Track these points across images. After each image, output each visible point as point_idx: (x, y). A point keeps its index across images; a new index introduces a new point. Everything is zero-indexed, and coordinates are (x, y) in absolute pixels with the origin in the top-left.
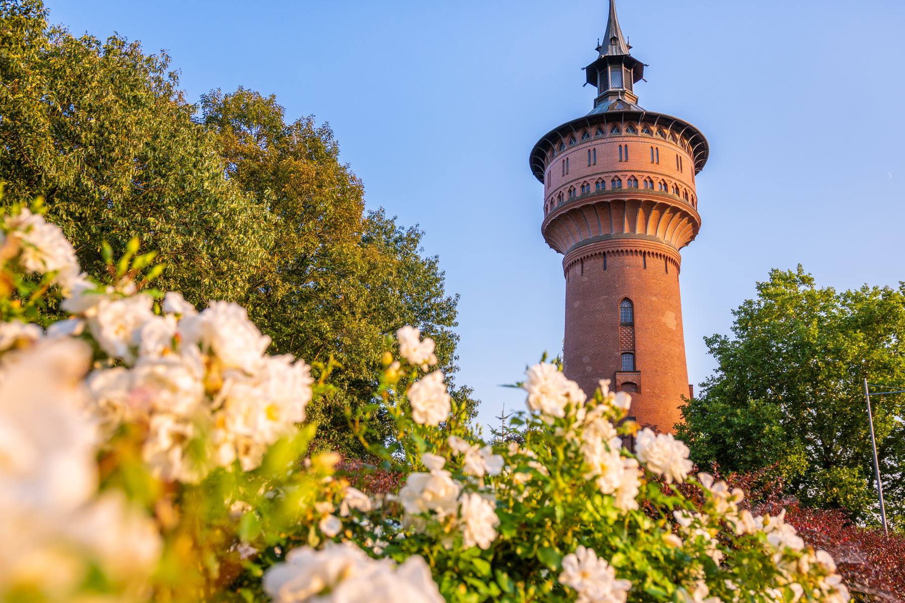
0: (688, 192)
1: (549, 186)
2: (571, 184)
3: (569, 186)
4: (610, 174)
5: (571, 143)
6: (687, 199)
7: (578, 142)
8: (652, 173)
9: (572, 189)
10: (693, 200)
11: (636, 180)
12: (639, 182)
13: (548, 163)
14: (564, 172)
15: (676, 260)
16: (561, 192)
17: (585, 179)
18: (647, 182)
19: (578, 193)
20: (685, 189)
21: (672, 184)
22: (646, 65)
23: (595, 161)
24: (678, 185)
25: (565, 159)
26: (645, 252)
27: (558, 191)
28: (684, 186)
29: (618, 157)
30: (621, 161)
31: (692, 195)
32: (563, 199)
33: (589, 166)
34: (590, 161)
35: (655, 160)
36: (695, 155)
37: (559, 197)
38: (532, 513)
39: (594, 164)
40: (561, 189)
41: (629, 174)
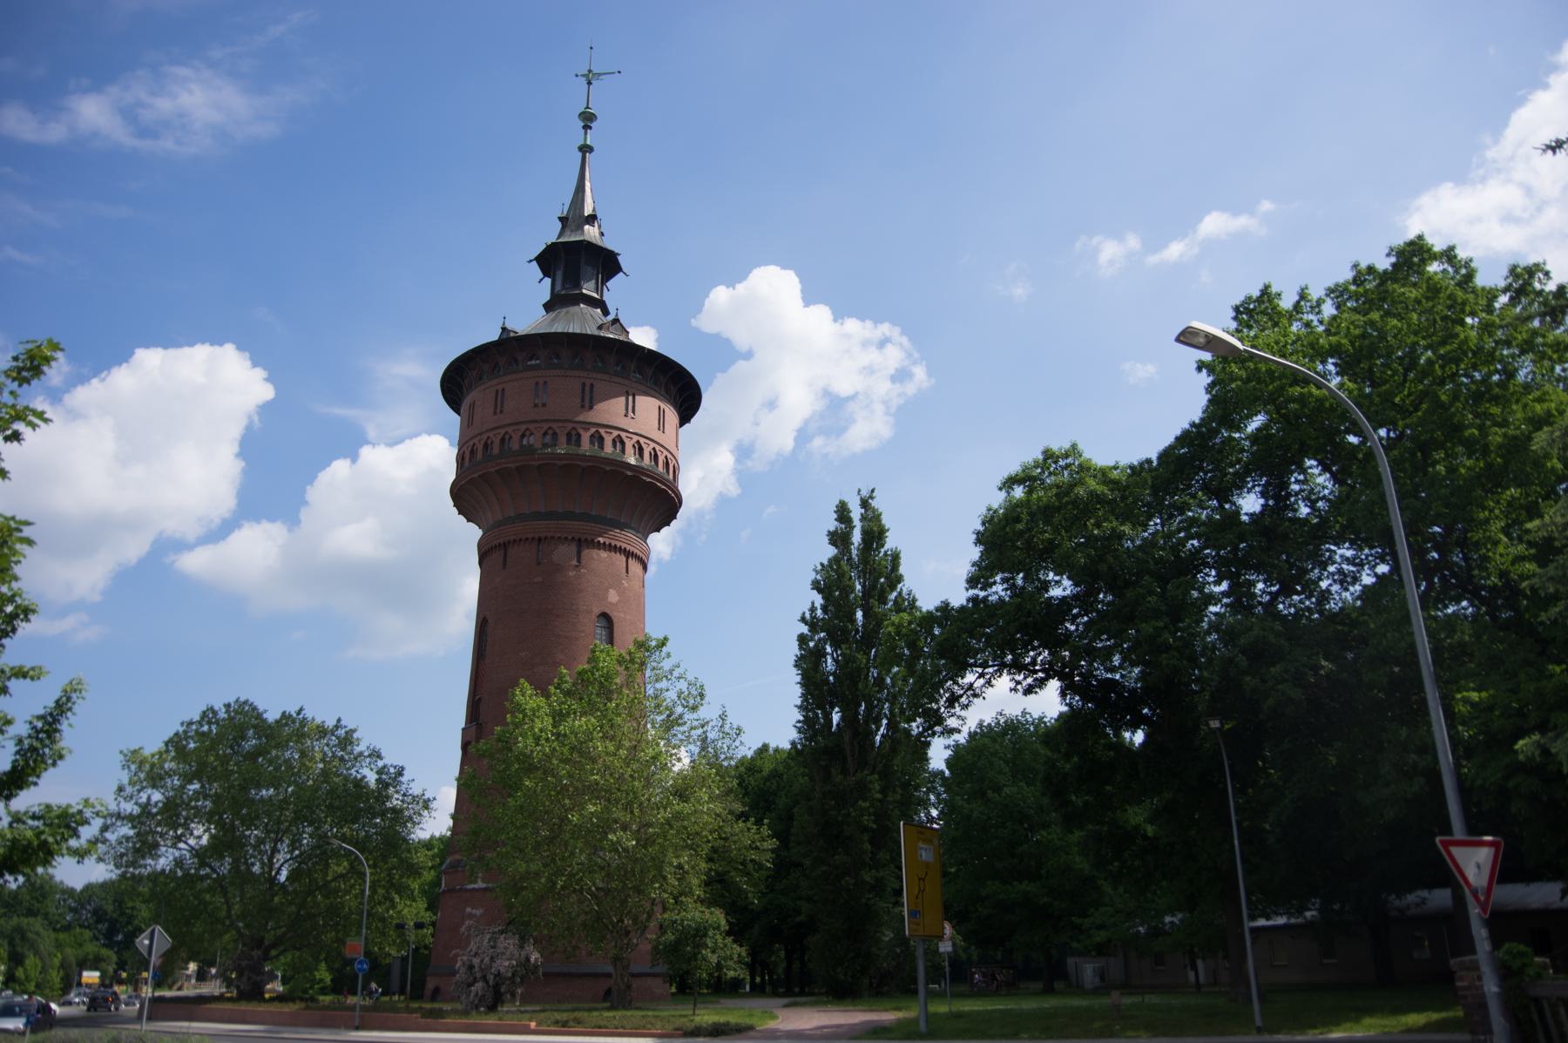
0: (659, 453)
2: (506, 429)
3: (502, 431)
6: (657, 463)
8: (662, 446)
9: (507, 437)
10: (667, 464)
11: (623, 443)
14: (496, 408)
15: (641, 555)
20: (654, 449)
21: (650, 449)
25: (500, 390)
26: (580, 539)
27: (471, 443)
28: (665, 453)
30: (583, 406)
31: (666, 457)
32: (492, 449)
36: (681, 406)
37: (486, 445)
38: (331, 980)
41: (616, 433)
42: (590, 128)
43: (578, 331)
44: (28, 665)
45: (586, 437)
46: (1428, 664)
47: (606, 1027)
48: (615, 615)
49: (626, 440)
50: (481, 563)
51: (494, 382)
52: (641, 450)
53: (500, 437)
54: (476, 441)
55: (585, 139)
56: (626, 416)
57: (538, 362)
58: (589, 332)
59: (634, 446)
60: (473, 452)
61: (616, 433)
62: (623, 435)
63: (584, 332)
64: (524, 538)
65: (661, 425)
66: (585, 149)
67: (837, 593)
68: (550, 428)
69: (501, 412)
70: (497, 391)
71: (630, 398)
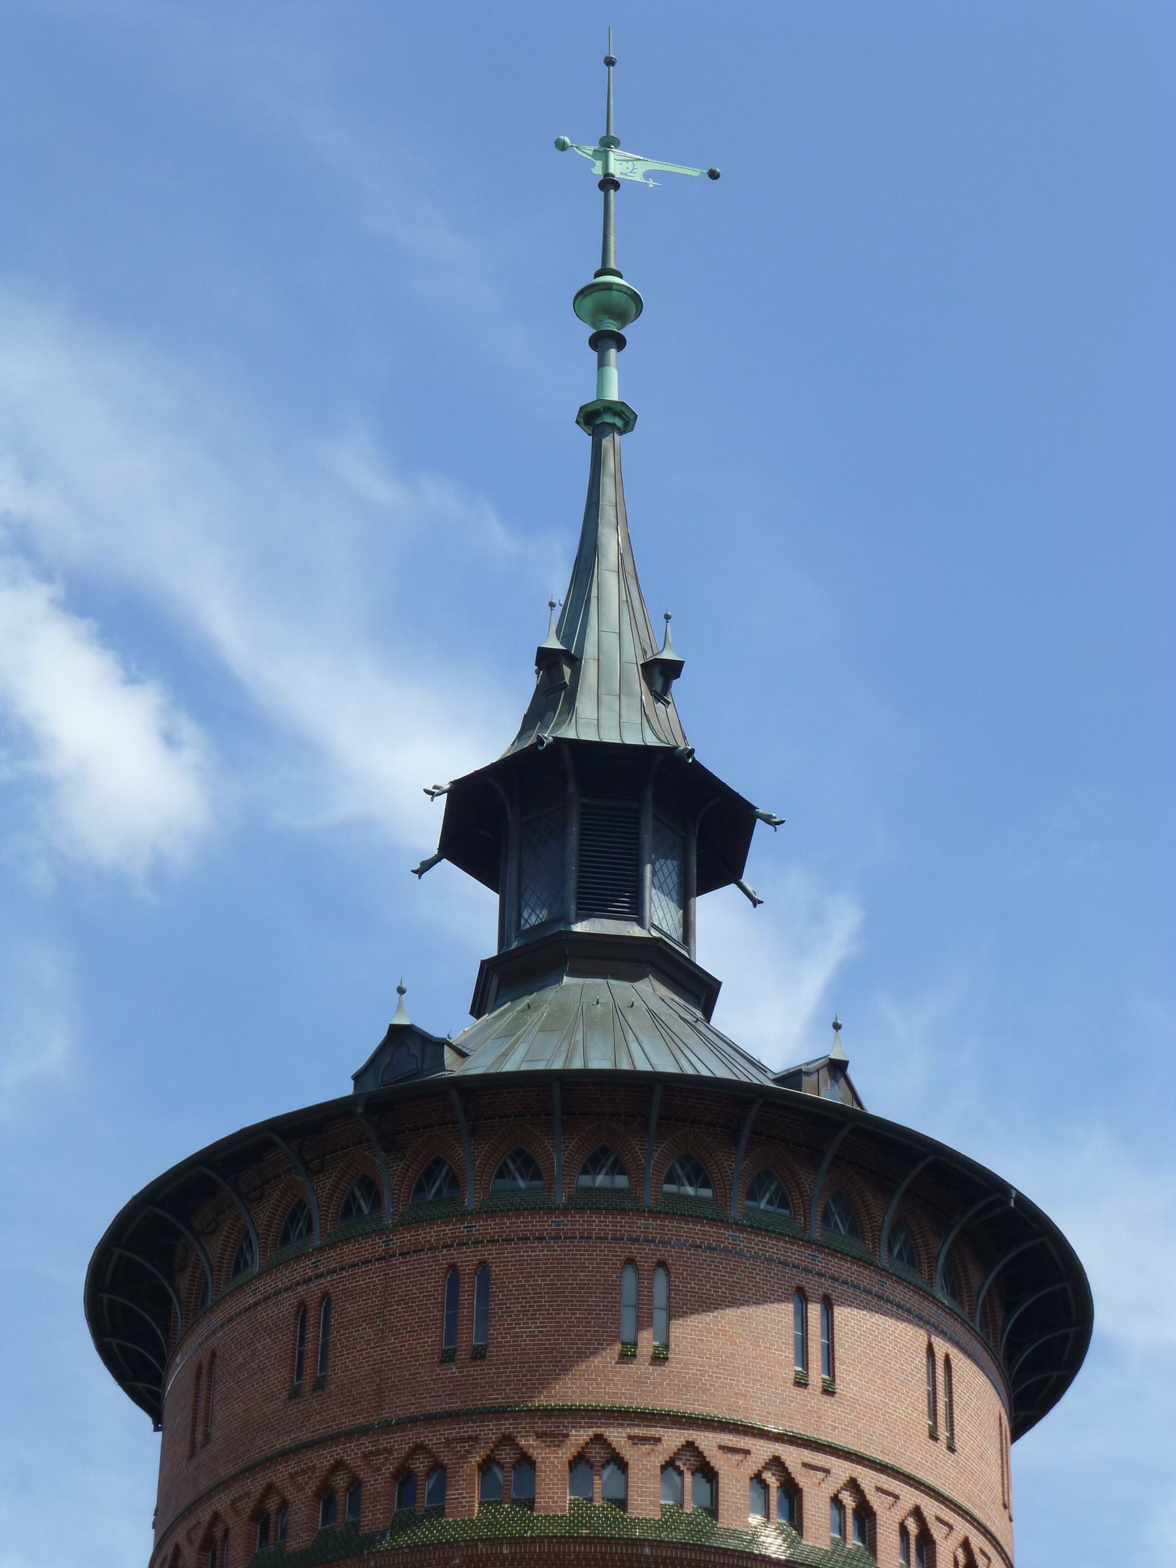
0: (937, 1532)
5: (348, 1210)
9: (341, 1481)
11: (708, 1473)
12: (723, 1480)
16: (270, 1489)
18: (765, 1486)
20: (917, 1513)
22: (768, 819)
24: (976, 1551)
28: (963, 1528)
31: (966, 1545)
33: (448, 1357)
34: (452, 1333)
35: (817, 1375)
37: (260, 1517)
39: (479, 1354)
40: (279, 1475)
41: (673, 1439)
49: (718, 1461)
51: (281, 1279)
52: (792, 1492)
53: (247, 1507)
54: (221, 1503)
56: (801, 1382)
57: (622, 1181)
58: (642, 1066)
59: (836, 1501)
61: (673, 1439)
62: (708, 1442)
63: (625, 1065)
67: (378, 1537)
68: (419, 1448)
69: (320, 1384)
70: (302, 1309)
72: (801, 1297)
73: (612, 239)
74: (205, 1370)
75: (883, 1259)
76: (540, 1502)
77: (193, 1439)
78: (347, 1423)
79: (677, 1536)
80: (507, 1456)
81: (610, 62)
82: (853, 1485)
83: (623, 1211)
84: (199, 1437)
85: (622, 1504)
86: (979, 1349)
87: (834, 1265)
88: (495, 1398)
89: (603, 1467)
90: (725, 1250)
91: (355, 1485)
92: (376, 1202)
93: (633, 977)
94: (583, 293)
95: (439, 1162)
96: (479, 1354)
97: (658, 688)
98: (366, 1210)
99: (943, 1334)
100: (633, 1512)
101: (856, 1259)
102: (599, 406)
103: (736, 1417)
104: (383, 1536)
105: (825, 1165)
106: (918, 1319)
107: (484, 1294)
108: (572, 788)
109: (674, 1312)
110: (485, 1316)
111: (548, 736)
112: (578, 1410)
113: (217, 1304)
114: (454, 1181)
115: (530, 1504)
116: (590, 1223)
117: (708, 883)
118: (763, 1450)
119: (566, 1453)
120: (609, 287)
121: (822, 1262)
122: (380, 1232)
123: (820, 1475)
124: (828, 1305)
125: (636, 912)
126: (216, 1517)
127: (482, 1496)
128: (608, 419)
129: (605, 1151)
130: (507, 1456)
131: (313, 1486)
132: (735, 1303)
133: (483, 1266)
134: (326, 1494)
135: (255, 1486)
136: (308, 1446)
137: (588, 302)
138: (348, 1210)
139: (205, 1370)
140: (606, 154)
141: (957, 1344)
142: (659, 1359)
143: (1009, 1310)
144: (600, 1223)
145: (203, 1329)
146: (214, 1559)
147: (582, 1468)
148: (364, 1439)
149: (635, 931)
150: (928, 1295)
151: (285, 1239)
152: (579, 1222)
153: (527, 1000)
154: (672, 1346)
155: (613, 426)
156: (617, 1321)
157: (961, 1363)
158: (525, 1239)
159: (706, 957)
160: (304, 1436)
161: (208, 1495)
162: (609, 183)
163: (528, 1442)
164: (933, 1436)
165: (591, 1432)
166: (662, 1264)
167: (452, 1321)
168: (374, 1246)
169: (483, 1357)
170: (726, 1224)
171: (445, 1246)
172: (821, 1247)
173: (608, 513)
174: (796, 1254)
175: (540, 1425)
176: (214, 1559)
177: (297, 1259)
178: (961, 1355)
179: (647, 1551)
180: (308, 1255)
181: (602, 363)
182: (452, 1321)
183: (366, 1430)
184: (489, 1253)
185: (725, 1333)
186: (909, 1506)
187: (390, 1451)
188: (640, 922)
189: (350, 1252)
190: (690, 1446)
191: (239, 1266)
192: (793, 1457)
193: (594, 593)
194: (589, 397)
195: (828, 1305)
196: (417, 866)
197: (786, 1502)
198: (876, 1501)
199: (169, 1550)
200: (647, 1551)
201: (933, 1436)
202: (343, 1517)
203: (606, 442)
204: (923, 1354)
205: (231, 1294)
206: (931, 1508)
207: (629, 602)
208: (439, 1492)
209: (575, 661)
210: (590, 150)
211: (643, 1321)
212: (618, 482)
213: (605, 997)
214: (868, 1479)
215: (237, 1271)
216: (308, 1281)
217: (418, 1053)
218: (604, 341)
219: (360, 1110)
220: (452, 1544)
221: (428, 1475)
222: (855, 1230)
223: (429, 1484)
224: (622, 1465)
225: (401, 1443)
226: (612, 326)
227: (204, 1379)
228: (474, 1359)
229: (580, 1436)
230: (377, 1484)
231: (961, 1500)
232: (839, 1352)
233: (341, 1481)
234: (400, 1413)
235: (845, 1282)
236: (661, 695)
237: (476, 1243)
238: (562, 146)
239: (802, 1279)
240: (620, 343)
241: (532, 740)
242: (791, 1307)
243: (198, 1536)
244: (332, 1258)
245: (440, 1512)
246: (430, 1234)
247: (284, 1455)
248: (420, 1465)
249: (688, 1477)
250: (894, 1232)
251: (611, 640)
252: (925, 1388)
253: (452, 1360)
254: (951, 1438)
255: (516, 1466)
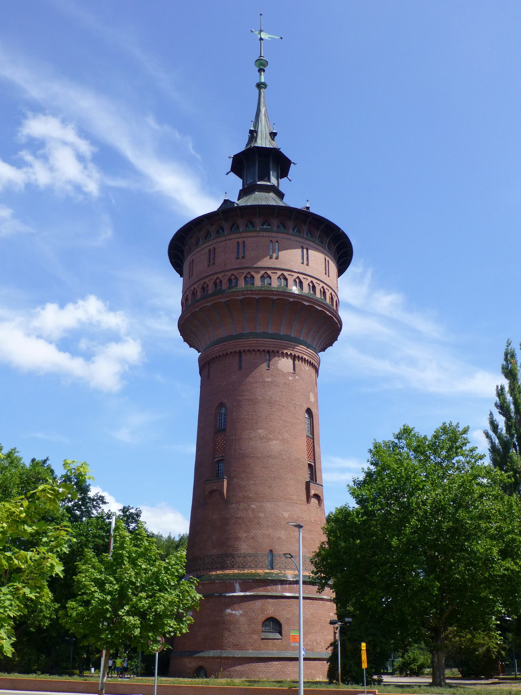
0: (326, 291)
1: (190, 275)
4: (226, 274)
5: (218, 232)
7: (226, 232)
9: (218, 281)
11: (286, 279)
13: (190, 251)
16: (205, 283)
17: (217, 275)
18: (296, 282)
19: (211, 289)
20: (323, 287)
22: (293, 163)
23: (244, 254)
24: (325, 289)
27: (192, 288)
28: (331, 291)
29: (235, 255)
31: (331, 294)
33: (238, 258)
34: (238, 254)
35: (305, 262)
37: (203, 288)
39: (243, 258)
40: (206, 280)
41: (279, 273)
42: (264, 71)
43: (257, 204)
44: (484, 435)
45: (257, 277)
46: (7, 677)
47: (425, 686)
48: (314, 411)
49: (287, 277)
50: (200, 373)
51: (206, 245)
52: (301, 283)
53: (200, 286)
55: (260, 79)
56: (303, 263)
59: (309, 285)
60: (194, 294)
61: (279, 273)
62: (286, 273)
64: (225, 353)
65: (327, 272)
66: (260, 86)
68: (233, 275)
69: (214, 264)
70: (210, 250)
71: (305, 251)
72: (303, 248)
73: (262, 50)
74: (191, 263)
75: (317, 242)
76: (255, 284)
77: (190, 275)
78: (219, 270)
79: (280, 290)
80: (249, 276)
81: (261, 15)
82: (312, 282)
83: (270, 232)
84: (191, 275)
85: (270, 284)
86: (333, 259)
87: (308, 242)
88: (246, 265)
89: (267, 278)
90: (289, 239)
91: (221, 282)
92: (223, 231)
93: (269, 192)
94: (257, 61)
95: (235, 223)
96: (243, 258)
97: (273, 138)
98: (221, 232)
99: (328, 256)
100: (272, 286)
101: (312, 242)
102: (260, 83)
103: (291, 269)
104: (226, 290)
105: (307, 224)
106: (323, 253)
107: (244, 247)
108: (257, 156)
109: (279, 250)
110: (244, 251)
111: (252, 145)
112: (262, 267)
113: (193, 250)
114: (238, 227)
115: (254, 284)
116: (264, 234)
117: (282, 177)
118: (296, 275)
119: (260, 275)
120: (262, 59)
121: (306, 242)
122: (224, 236)
123: (306, 280)
124: (307, 249)
125: (269, 181)
126: (195, 288)
127: (244, 283)
128: (262, 86)
129: (266, 221)
130: (249, 276)
131: (213, 282)
132: (290, 249)
133: (244, 242)
134: (215, 283)
135: (202, 282)
136: (212, 275)
137: (258, 63)
138: (218, 232)
139: (191, 263)
140: (261, 33)
141: (330, 258)
142: (277, 258)
143: (338, 254)
144: (265, 234)
145: (190, 256)
146: (194, 296)
147: (263, 278)
148: (223, 273)
149: (269, 184)
150: (325, 249)
151: (206, 238)
152: (262, 234)
153: (249, 197)
154: (279, 256)
155: (263, 87)
156: (269, 252)
157: (330, 261)
158: (252, 237)
159: (281, 189)
160: (211, 273)
161: (193, 285)
162: (261, 39)
163: (253, 273)
164: (326, 274)
165: (264, 272)
166: (277, 241)
167: (238, 252)
168: (223, 238)
169: (244, 258)
170: (289, 235)
171: (237, 238)
172: (306, 239)
173: (262, 104)
174: (302, 240)
175: (255, 270)
176: (194, 296)
177: (208, 241)
178: (330, 260)
179: (275, 292)
180: (210, 241)
181: (260, 75)
182: (238, 252)
183: (223, 271)
184: (244, 239)
185: (289, 254)
186: (322, 286)
187: (227, 275)
188: (270, 182)
189: (219, 240)
190: (283, 274)
191: (197, 244)
192: (301, 276)
193: (260, 119)
194: (258, 81)
195: (307, 249)
196: (226, 173)
197: (300, 285)
198: (316, 285)
199: (185, 295)
200: (275, 292)
201: (326, 274)
202: (219, 287)
203: (262, 90)
204: (324, 259)
205: (196, 249)
206: (325, 287)
207: (267, 121)
208: (236, 283)
209: (256, 132)
210: (257, 32)
211: (274, 252)
212: (264, 98)
213: (264, 195)
214: (315, 281)
215: (197, 245)
216: (210, 245)
217: (229, 205)
218: (261, 70)
219: (220, 213)
220: (239, 291)
221: (234, 280)
222: (312, 237)
223: (234, 281)
224: (270, 278)
225: (229, 274)
226: (262, 67)
227: (191, 264)
228: (242, 258)
229: (262, 272)
230: (225, 281)
231: (330, 286)
232: (309, 258)
233: (218, 281)
234: (229, 268)
235: (310, 246)
236: (273, 139)
237: (242, 238)
238: (252, 31)
239: (303, 245)
240: (264, 71)
241: (249, 146)
242: (301, 249)
243: (191, 293)
244: (215, 241)
245: (237, 286)
246: (234, 236)
247: (207, 277)
248: (233, 278)
249: (282, 279)
250: (319, 237)
251: (263, 128)
252: (324, 265)
253: (238, 259)
254: (329, 275)
255: (251, 278)
